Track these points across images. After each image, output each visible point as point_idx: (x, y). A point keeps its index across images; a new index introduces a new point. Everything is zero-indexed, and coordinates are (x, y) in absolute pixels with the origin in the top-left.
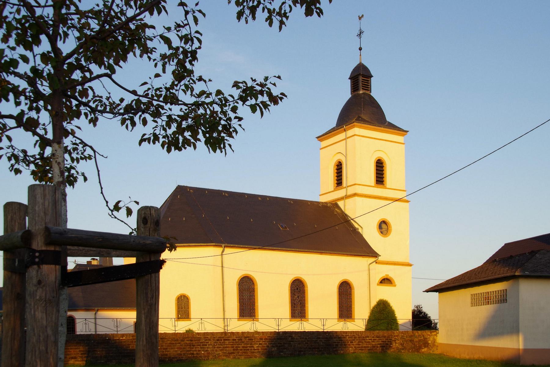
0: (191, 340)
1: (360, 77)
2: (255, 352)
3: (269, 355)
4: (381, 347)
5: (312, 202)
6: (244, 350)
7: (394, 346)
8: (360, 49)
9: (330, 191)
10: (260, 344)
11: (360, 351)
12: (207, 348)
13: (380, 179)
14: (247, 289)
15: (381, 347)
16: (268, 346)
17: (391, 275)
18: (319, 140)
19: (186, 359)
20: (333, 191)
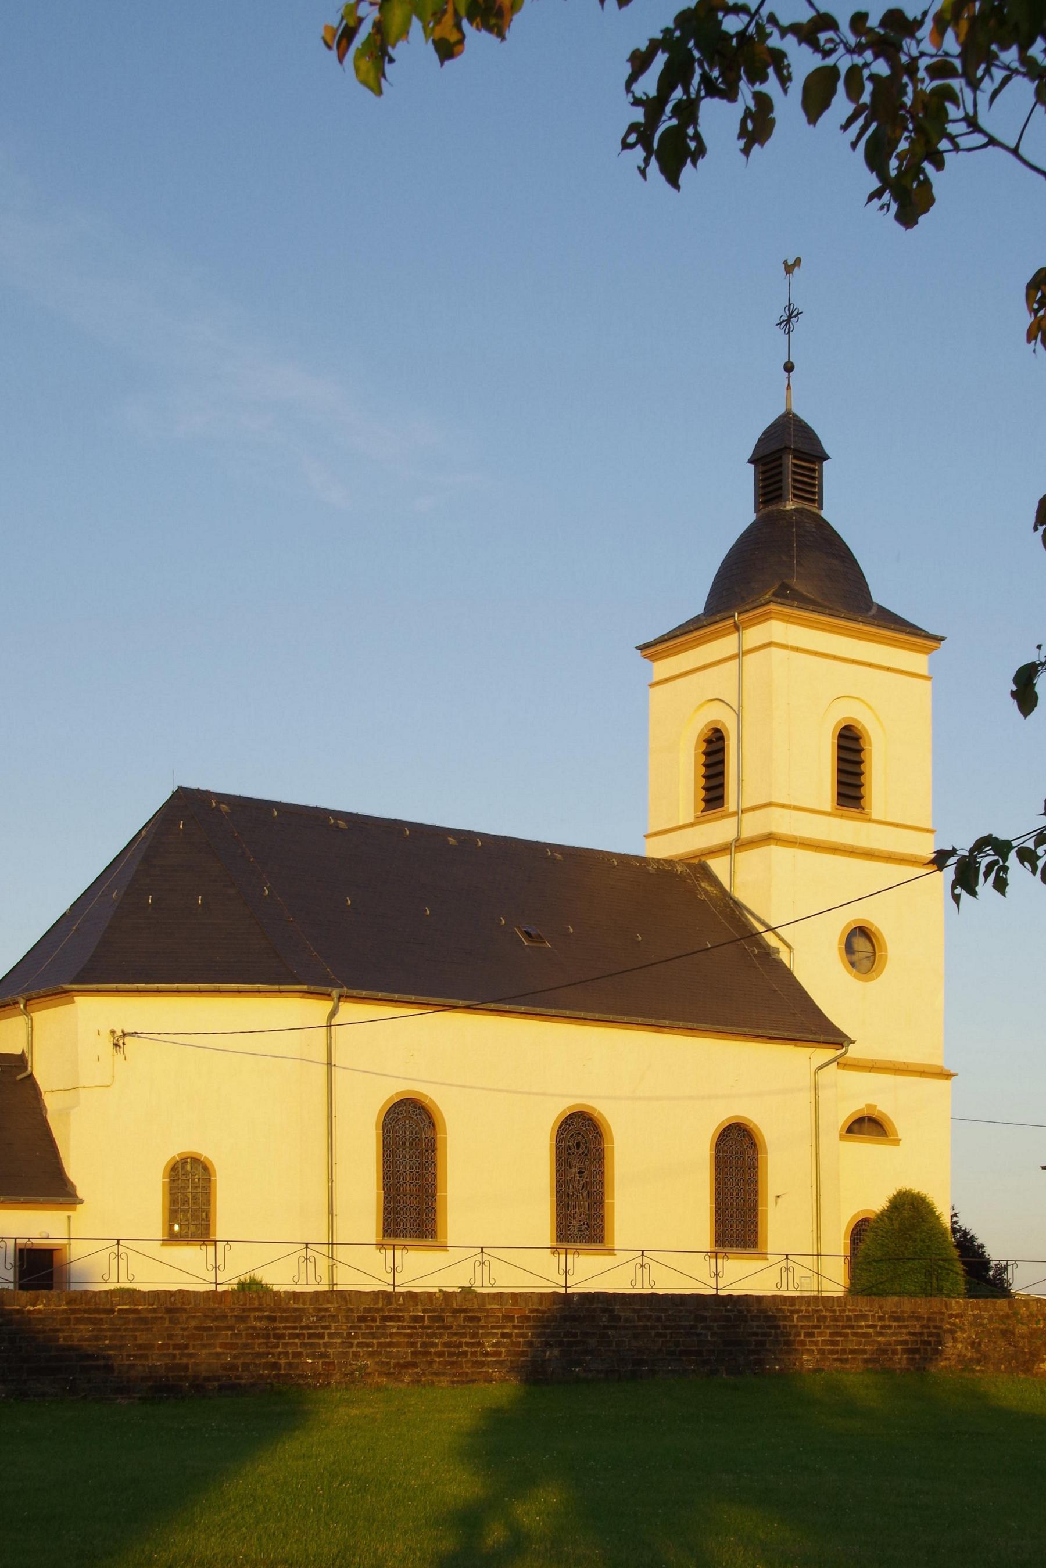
0: (273, 1319)
1: (787, 459)
2: (488, 1364)
3: (535, 1373)
4: (905, 1351)
5: (623, 858)
6: (451, 1354)
7: (949, 1352)
8: (789, 368)
9: (681, 823)
10: (503, 1335)
11: (837, 1364)
12: (325, 1345)
13: (850, 789)
14: (410, 1138)
15: (905, 1351)
16: (530, 1344)
17: (885, 1108)
18: (647, 657)
19: (253, 1385)
20: (692, 825)
